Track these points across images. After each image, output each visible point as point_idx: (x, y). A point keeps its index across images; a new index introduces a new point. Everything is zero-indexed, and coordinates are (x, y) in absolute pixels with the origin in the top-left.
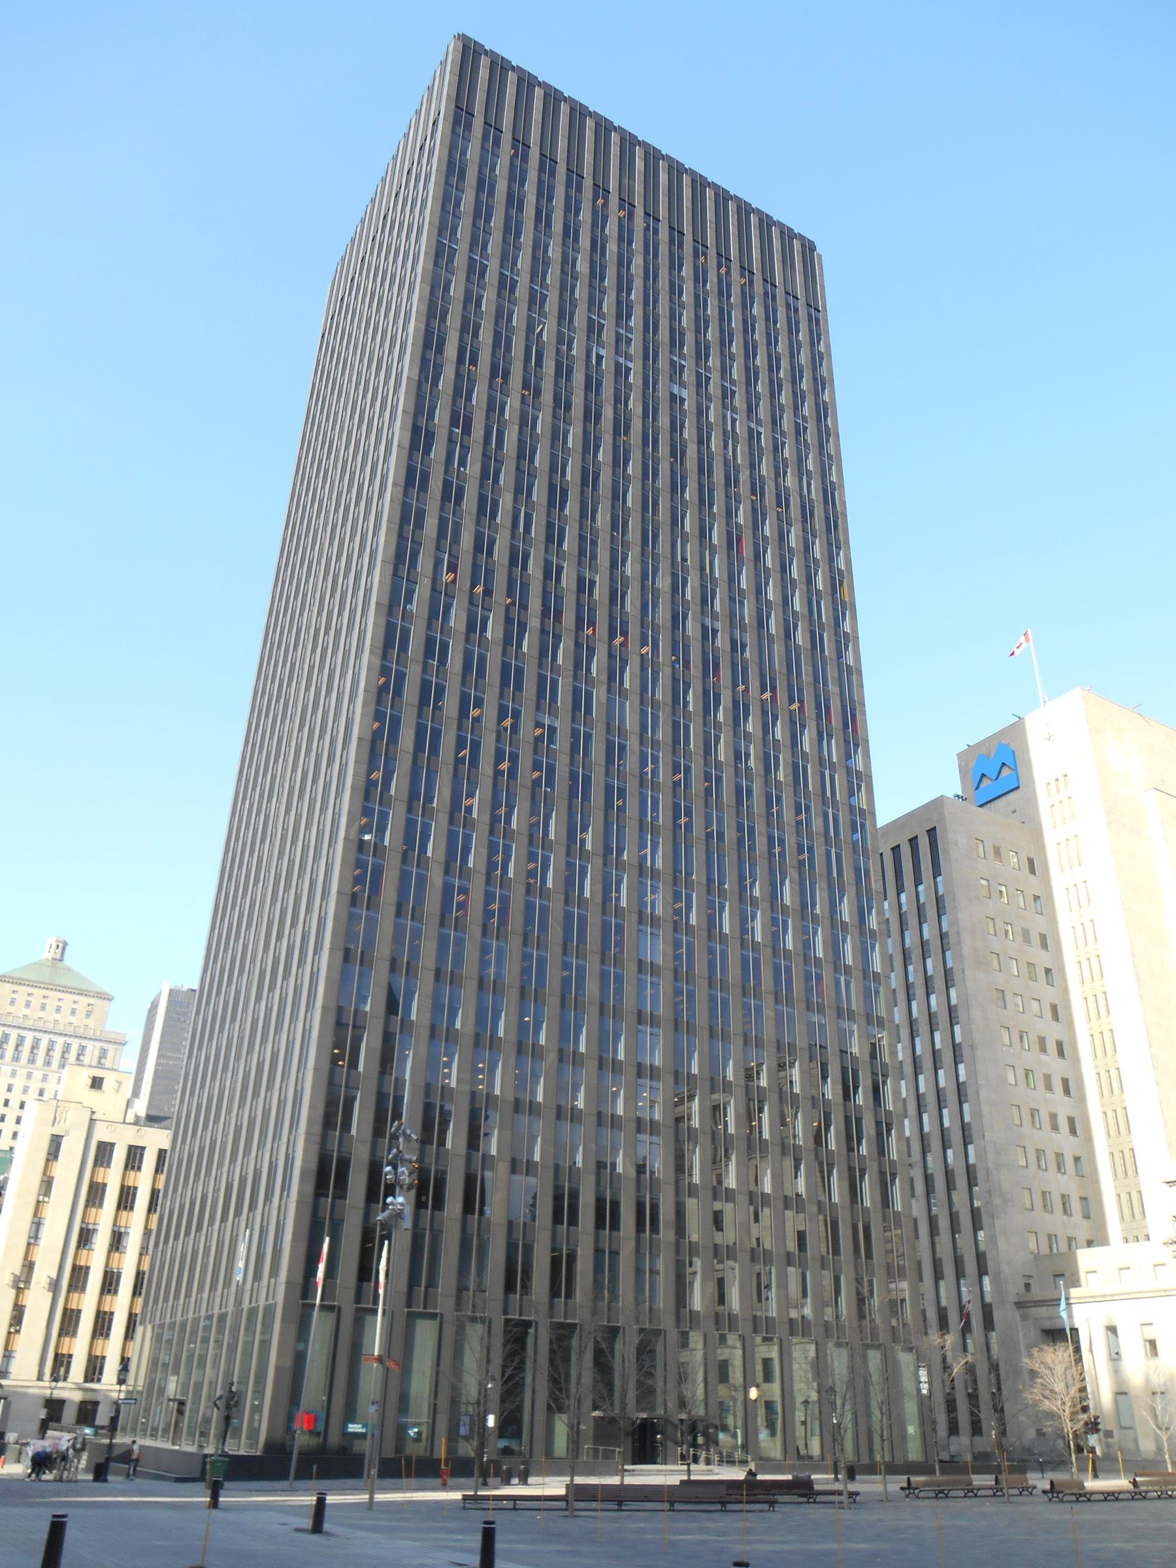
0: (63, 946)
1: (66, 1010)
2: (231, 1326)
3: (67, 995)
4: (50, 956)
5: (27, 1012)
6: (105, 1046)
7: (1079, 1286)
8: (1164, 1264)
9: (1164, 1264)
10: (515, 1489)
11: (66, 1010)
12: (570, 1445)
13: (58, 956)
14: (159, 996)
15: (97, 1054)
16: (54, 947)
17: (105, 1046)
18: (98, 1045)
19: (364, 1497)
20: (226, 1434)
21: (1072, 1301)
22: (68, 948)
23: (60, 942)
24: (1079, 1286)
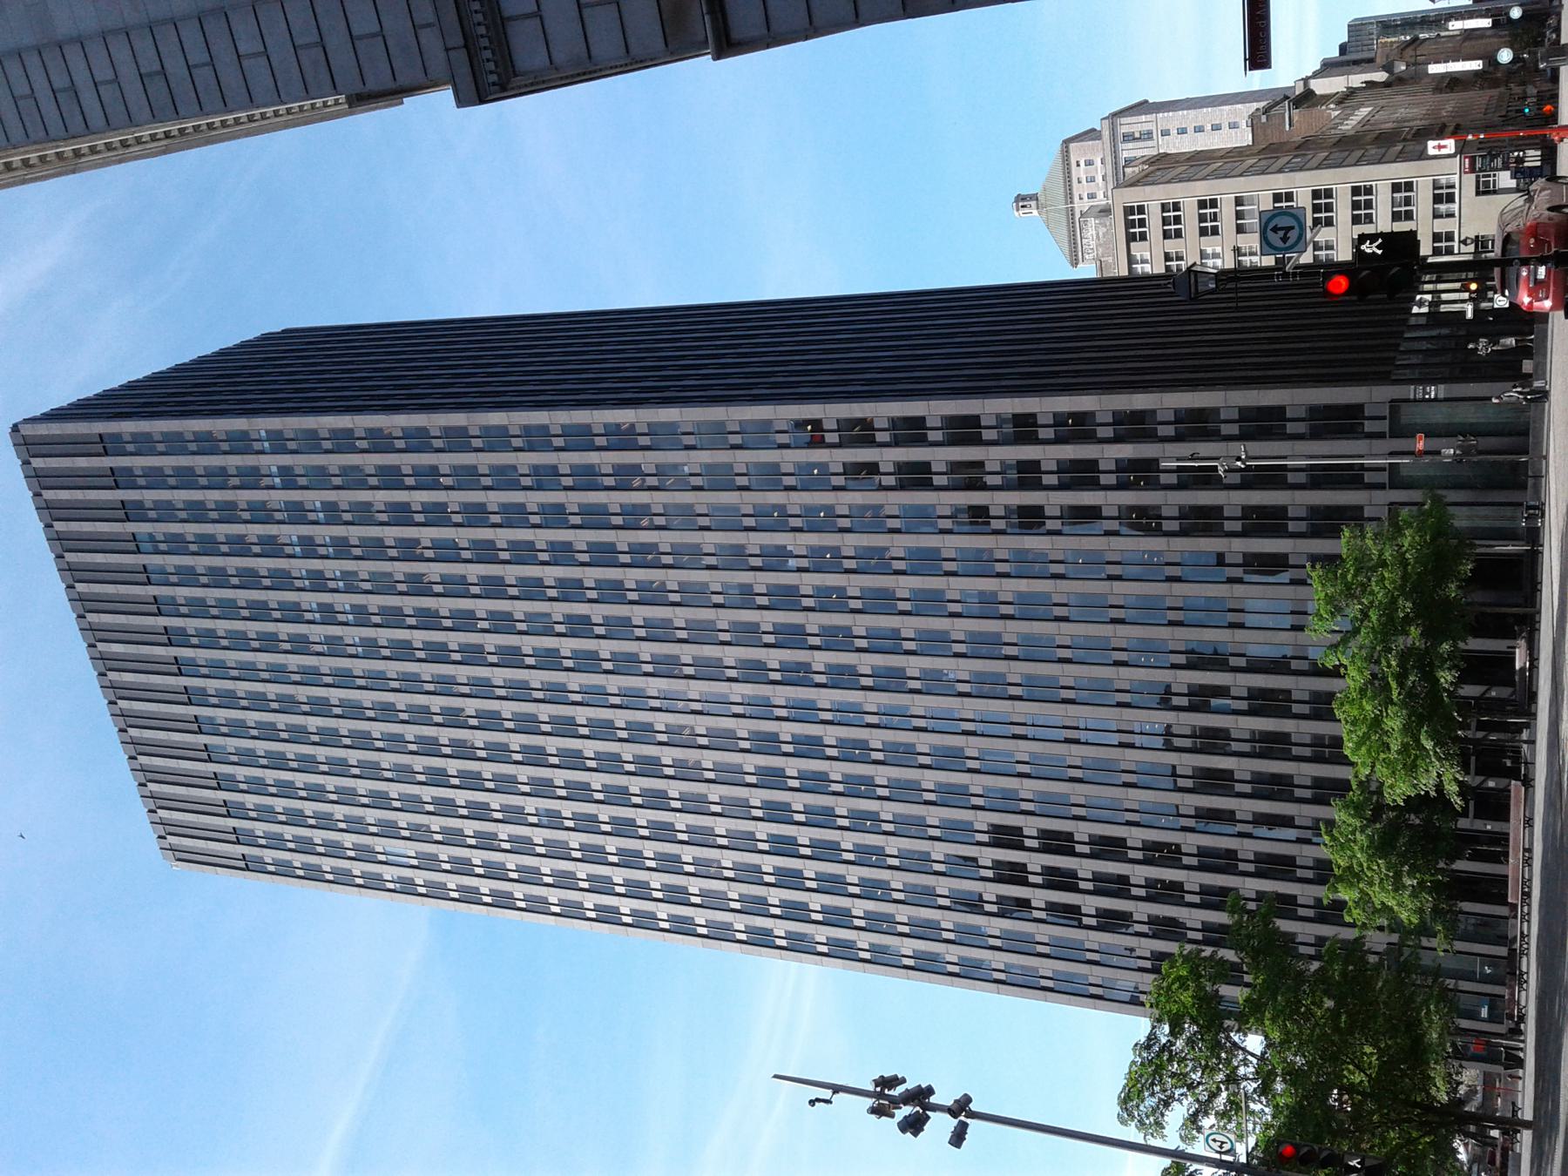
0: (1022, 200)
1: (1091, 188)
2: (1557, 1134)
3: (1075, 190)
4: (1035, 212)
5: (1099, 179)
6: (1120, 138)
7: (1270, 67)
8: (776, 1076)
9: (776, 1076)
10: (1552, 284)
11: (1091, 188)
12: (1419, 16)
13: (1033, 203)
14: (903, 1081)
15: (1130, 145)
16: (1026, 210)
17: (1120, 138)
18: (1121, 146)
19: (1433, 35)
20: (1510, 434)
21: (1412, 397)
22: (1024, 192)
23: (1017, 206)
24: (1270, 67)
